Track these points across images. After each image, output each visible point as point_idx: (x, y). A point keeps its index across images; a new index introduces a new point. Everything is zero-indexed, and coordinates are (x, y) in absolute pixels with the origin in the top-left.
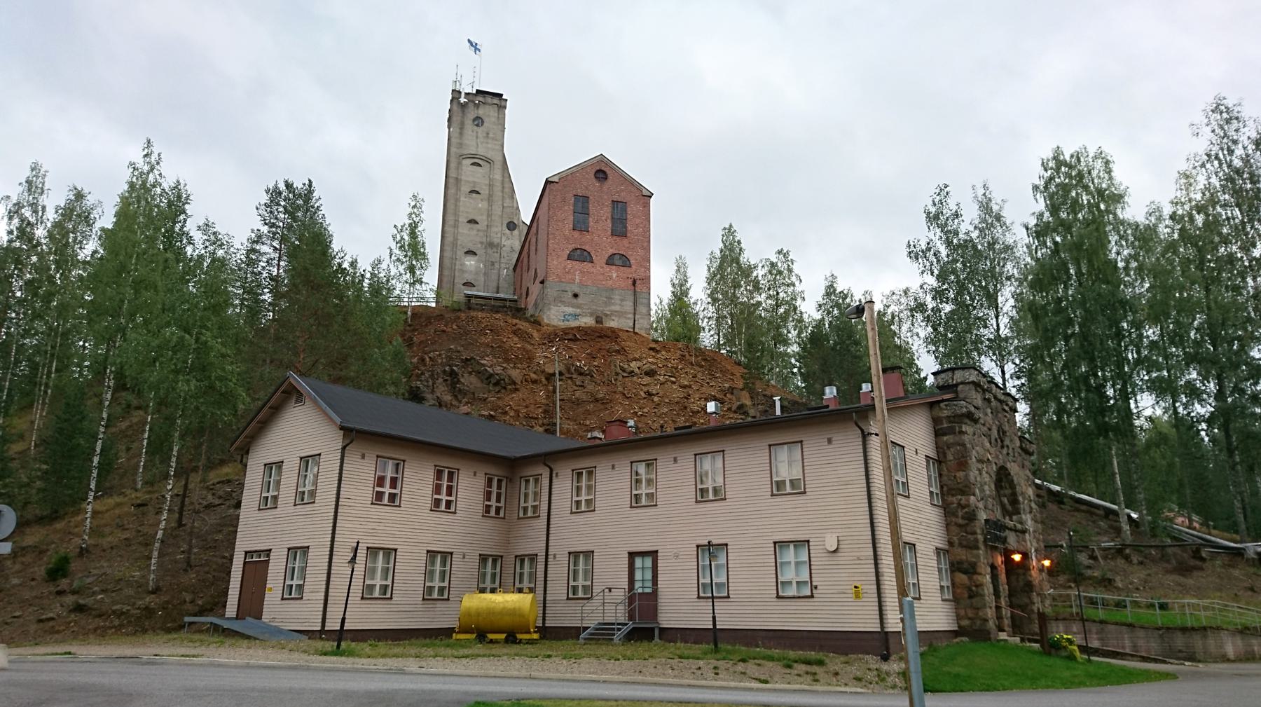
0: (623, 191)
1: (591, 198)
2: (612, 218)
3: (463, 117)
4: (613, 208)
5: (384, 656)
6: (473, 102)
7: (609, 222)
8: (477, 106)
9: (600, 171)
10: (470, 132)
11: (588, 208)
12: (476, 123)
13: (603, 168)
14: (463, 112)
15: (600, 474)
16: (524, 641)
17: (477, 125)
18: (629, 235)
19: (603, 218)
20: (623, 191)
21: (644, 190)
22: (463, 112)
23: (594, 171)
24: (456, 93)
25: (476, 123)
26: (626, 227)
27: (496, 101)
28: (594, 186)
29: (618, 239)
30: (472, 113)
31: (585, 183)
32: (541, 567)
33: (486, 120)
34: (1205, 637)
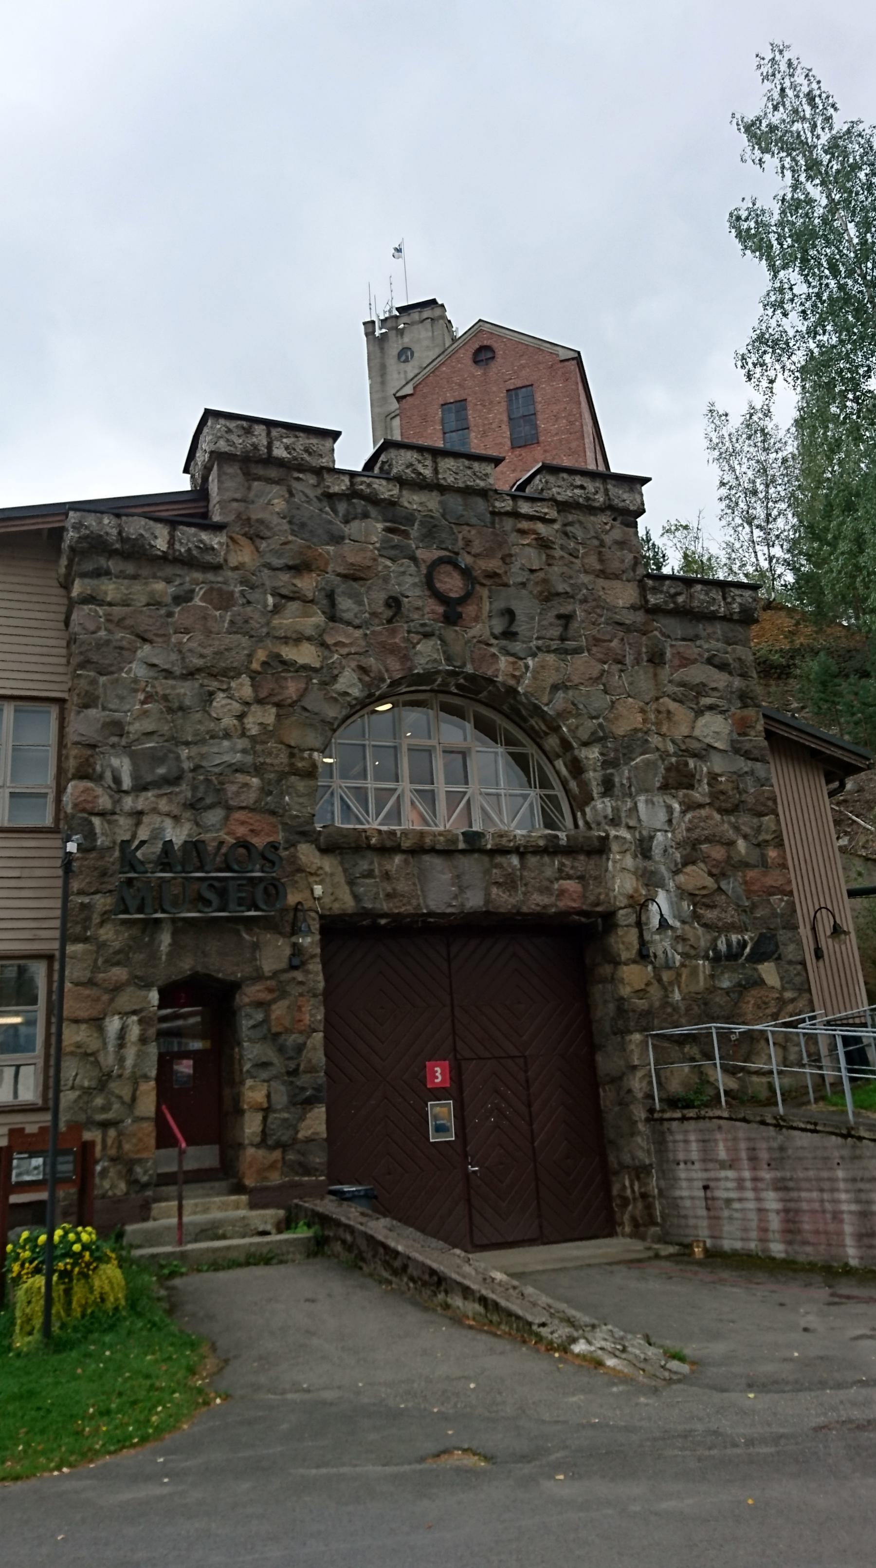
0: (523, 367)
1: (469, 399)
2: (510, 419)
3: (382, 357)
4: (510, 401)
5: (629, 1429)
6: (396, 328)
7: (505, 428)
8: (401, 333)
9: (483, 349)
10: (395, 376)
11: (466, 419)
12: (403, 358)
13: (485, 343)
14: (382, 349)
15: (481, 903)
16: (412, 1270)
17: (406, 361)
18: (542, 438)
19: (493, 426)
20: (523, 367)
21: (561, 352)
22: (382, 349)
23: (470, 354)
24: (369, 325)
25: (403, 358)
26: (535, 427)
27: (427, 313)
28: (473, 376)
29: (523, 452)
30: (394, 347)
31: (456, 379)
32: (57, 966)
33: (415, 348)
34: (661, 1124)
